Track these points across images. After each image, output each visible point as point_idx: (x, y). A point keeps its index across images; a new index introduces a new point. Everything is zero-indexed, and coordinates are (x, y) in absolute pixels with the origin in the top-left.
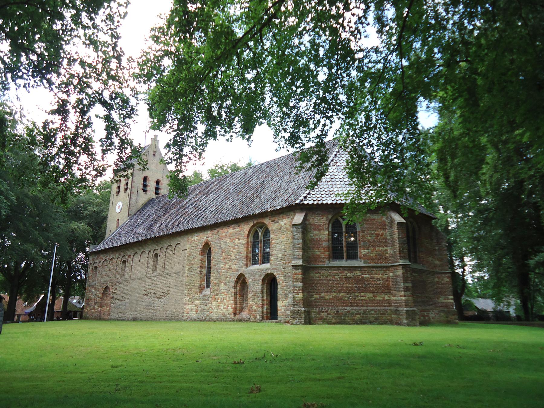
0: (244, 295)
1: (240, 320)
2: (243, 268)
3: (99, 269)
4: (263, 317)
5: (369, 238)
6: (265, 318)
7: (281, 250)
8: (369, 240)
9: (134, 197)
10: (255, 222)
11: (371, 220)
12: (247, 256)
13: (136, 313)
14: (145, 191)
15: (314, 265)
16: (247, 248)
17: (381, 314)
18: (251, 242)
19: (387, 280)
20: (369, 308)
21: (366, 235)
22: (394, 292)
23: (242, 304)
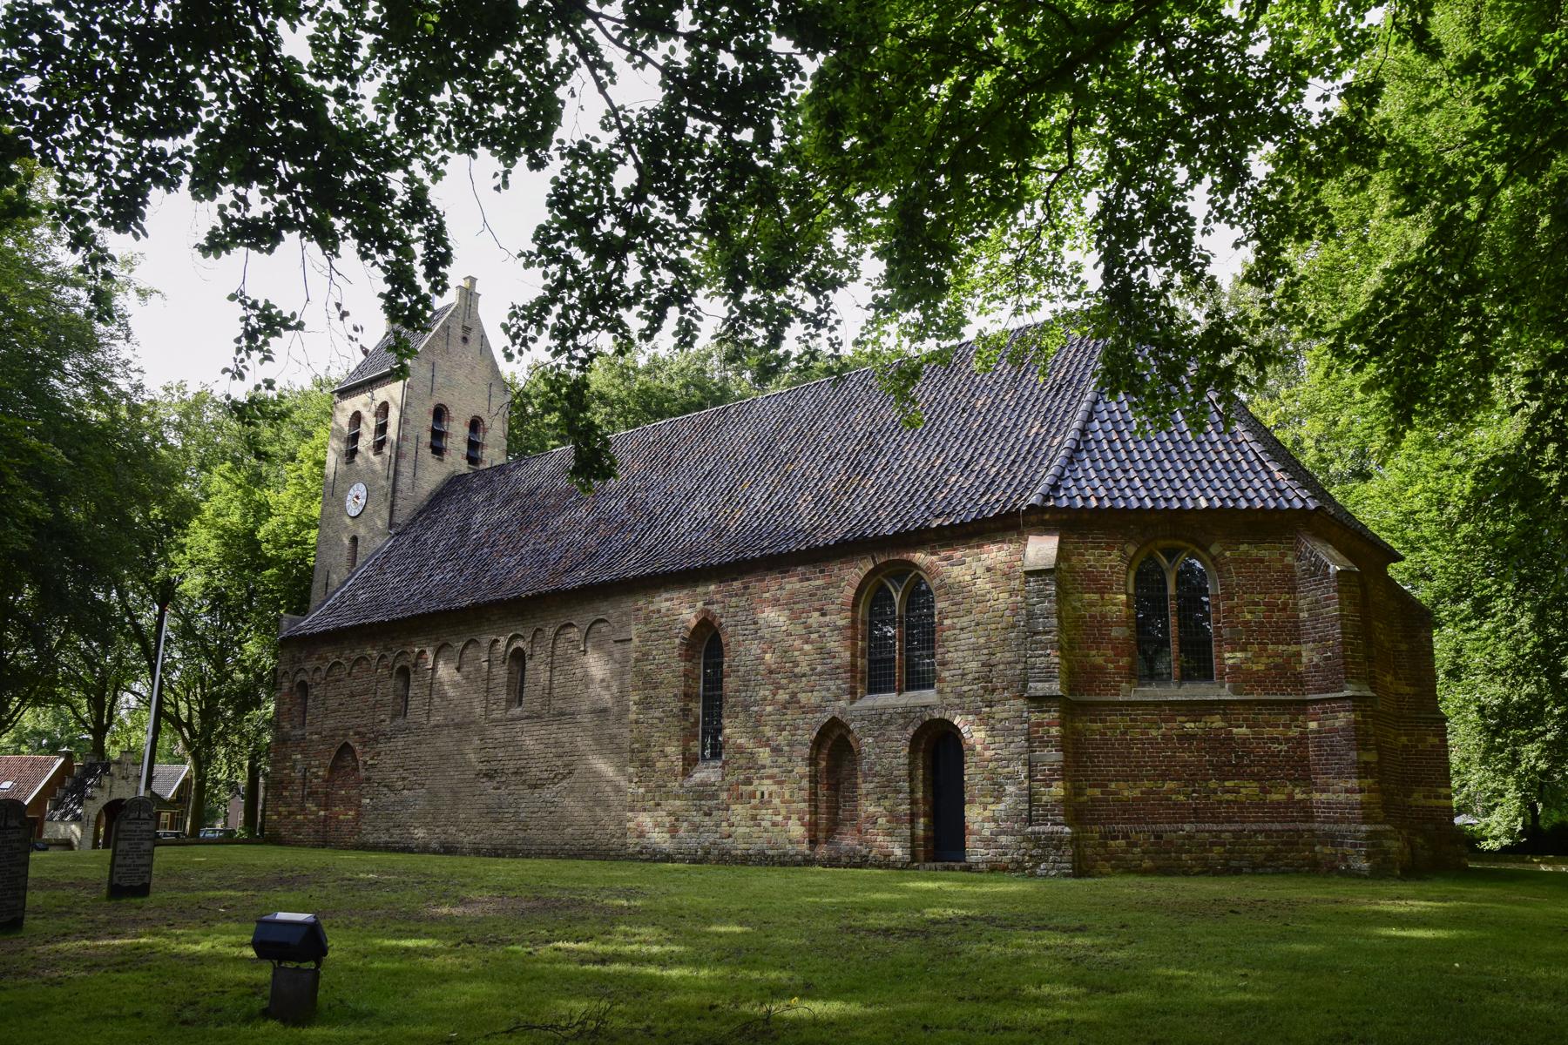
0: (838, 783)
1: (833, 862)
2: (842, 703)
3: (315, 691)
4: (914, 855)
5: (1249, 617)
6: (921, 856)
7: (976, 649)
8: (1247, 623)
9: (406, 468)
10: (881, 560)
11: (1253, 561)
12: (854, 665)
13: (452, 830)
14: (438, 450)
15: (1085, 698)
16: (854, 639)
17: (1284, 843)
18: (863, 623)
19: (1302, 740)
20: (1248, 826)
21: (1238, 605)
22: (1321, 780)
23: (833, 809)
